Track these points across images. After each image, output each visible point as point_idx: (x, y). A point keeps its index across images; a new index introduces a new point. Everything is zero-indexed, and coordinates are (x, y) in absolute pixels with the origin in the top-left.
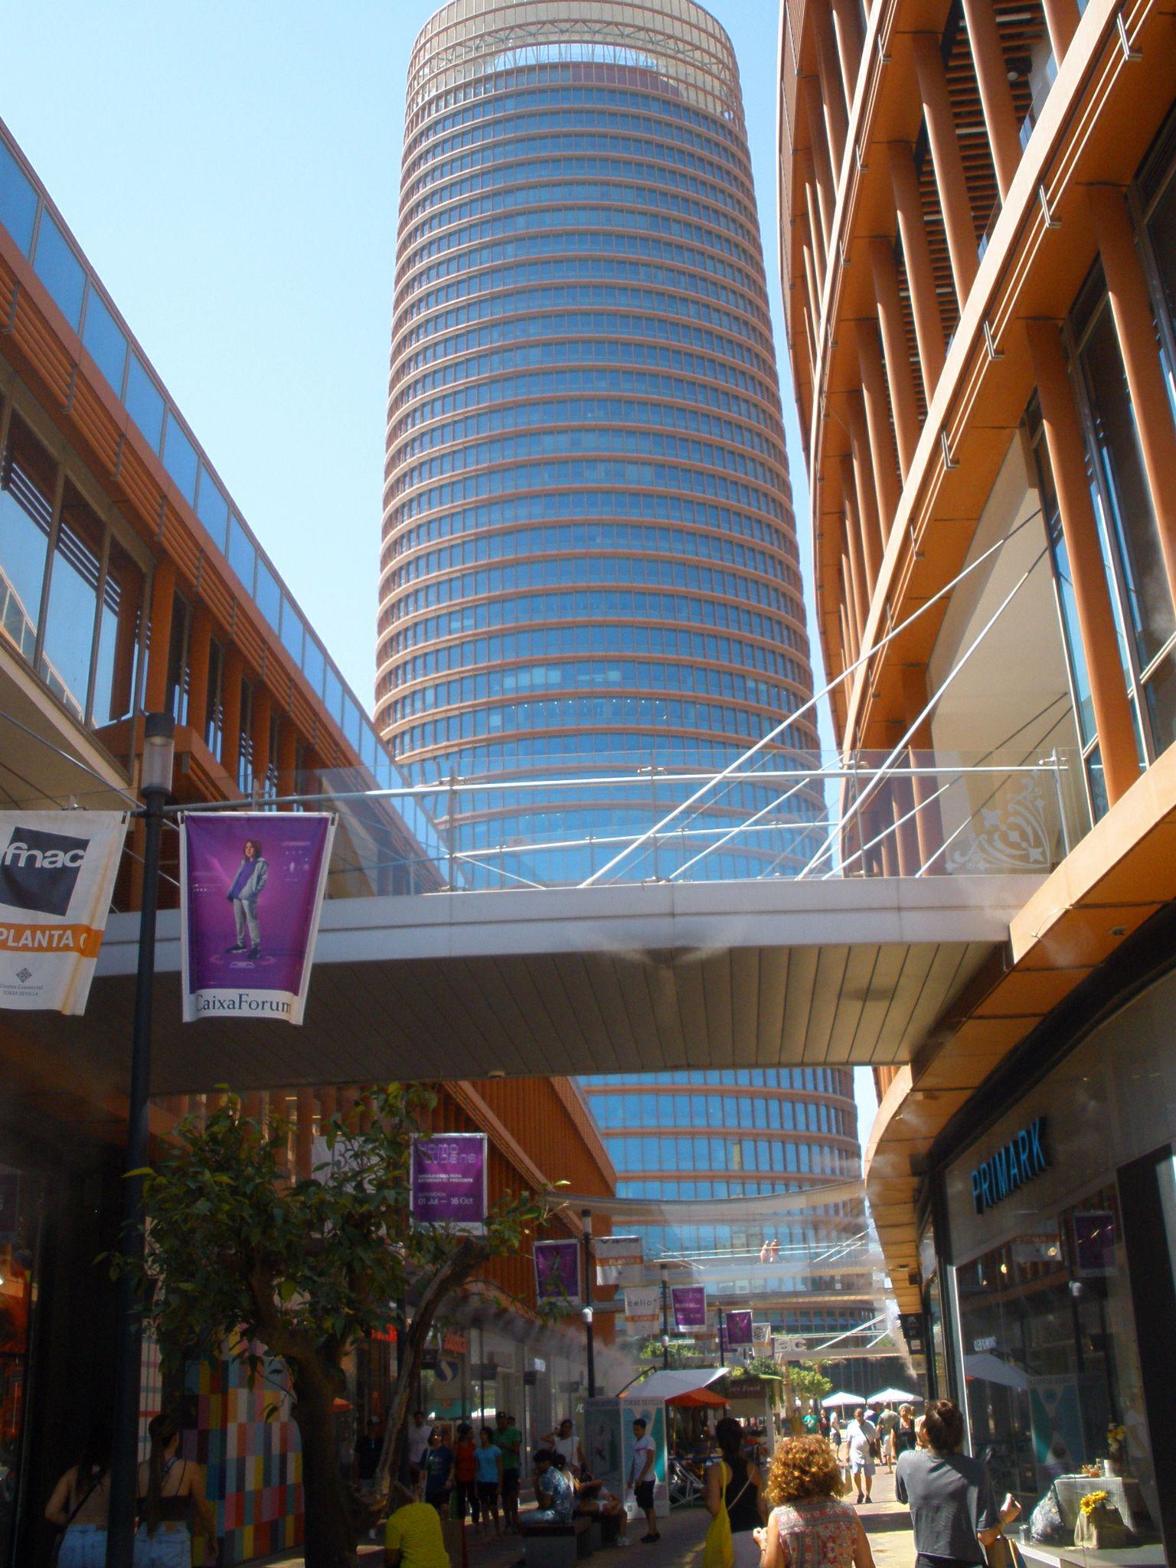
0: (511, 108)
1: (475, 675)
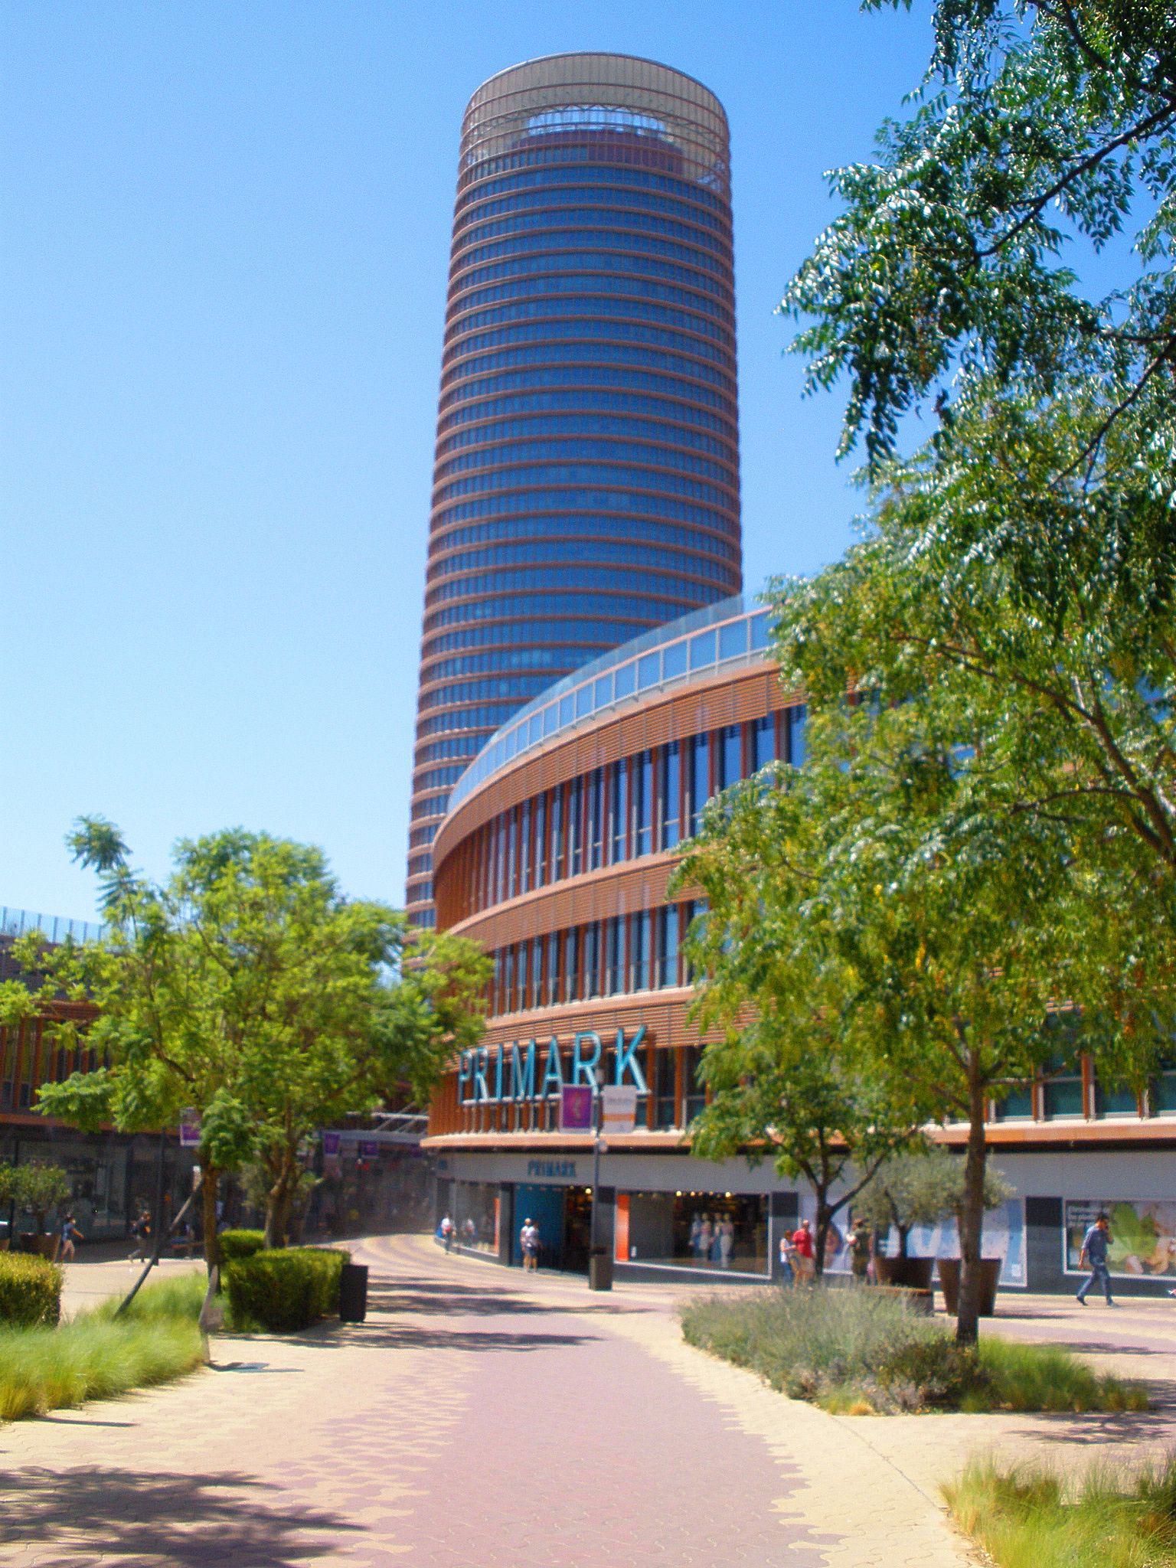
0: (539, 181)
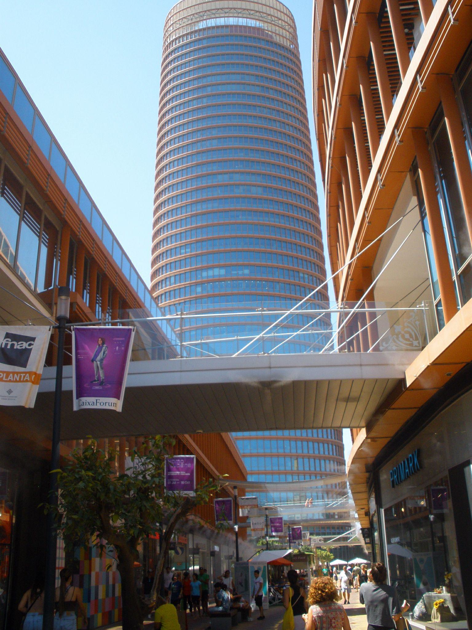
0: (205, 43)
1: (191, 271)
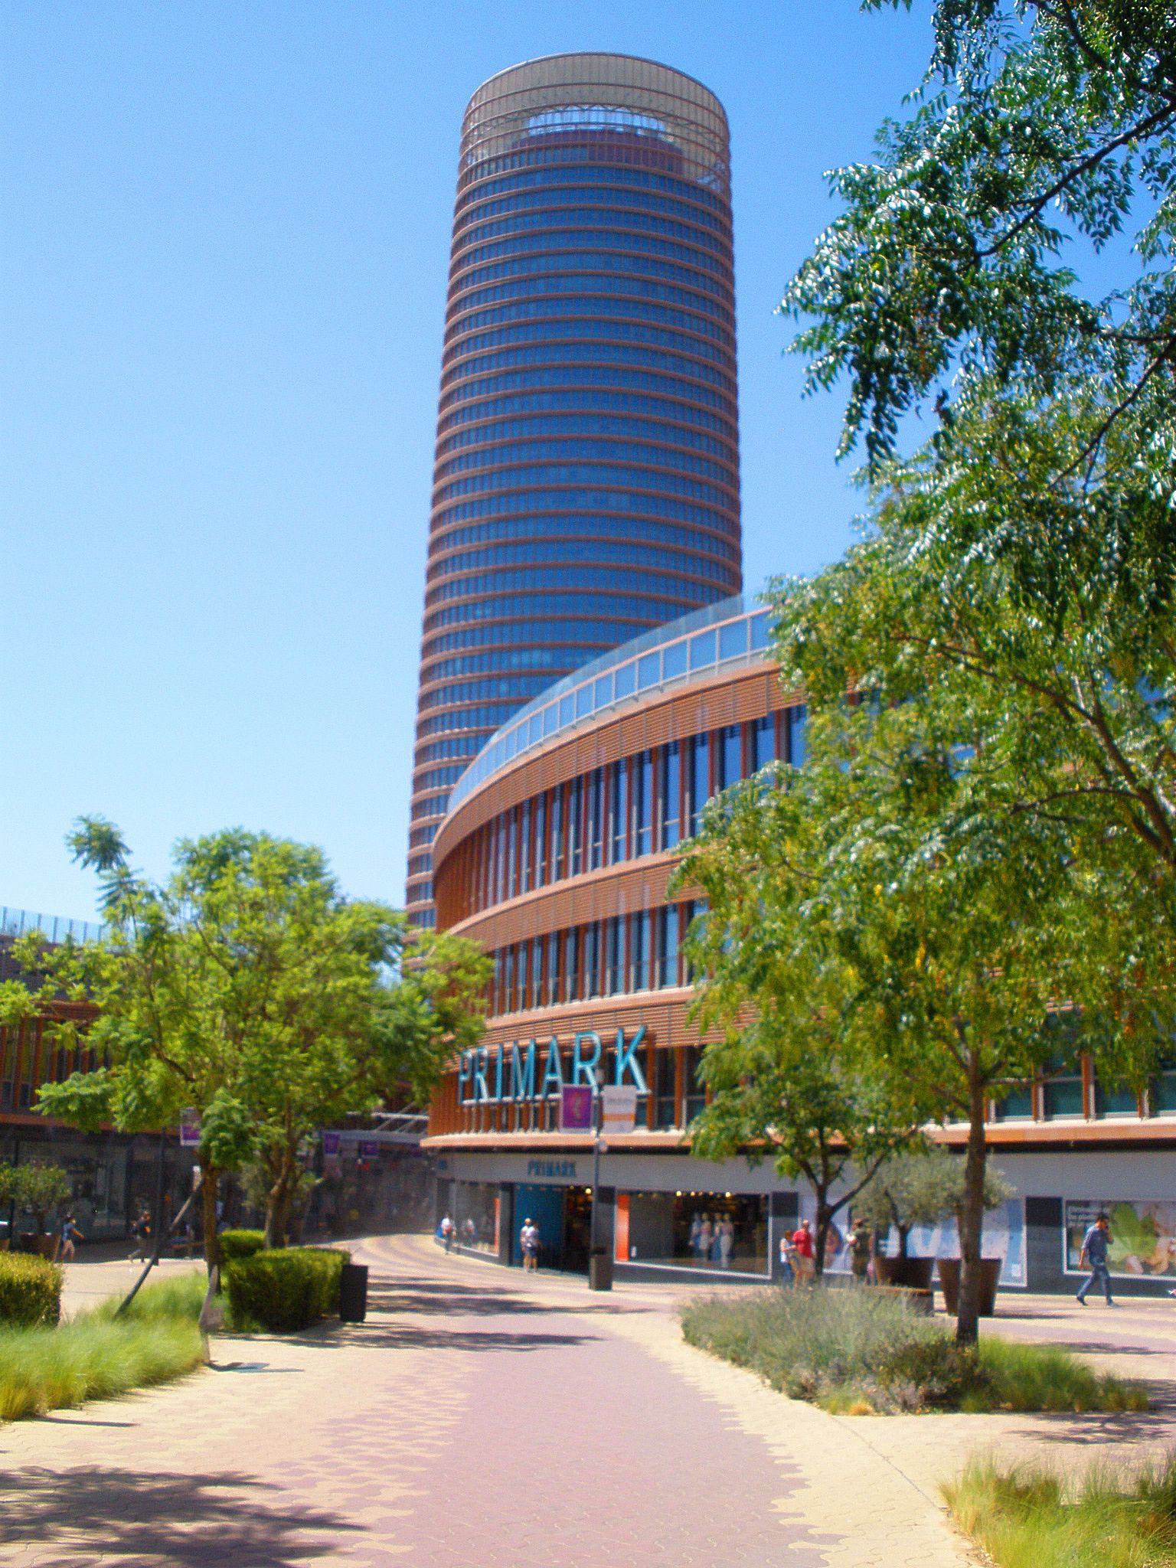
0: (539, 181)
